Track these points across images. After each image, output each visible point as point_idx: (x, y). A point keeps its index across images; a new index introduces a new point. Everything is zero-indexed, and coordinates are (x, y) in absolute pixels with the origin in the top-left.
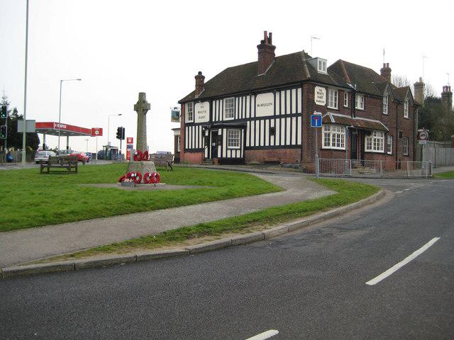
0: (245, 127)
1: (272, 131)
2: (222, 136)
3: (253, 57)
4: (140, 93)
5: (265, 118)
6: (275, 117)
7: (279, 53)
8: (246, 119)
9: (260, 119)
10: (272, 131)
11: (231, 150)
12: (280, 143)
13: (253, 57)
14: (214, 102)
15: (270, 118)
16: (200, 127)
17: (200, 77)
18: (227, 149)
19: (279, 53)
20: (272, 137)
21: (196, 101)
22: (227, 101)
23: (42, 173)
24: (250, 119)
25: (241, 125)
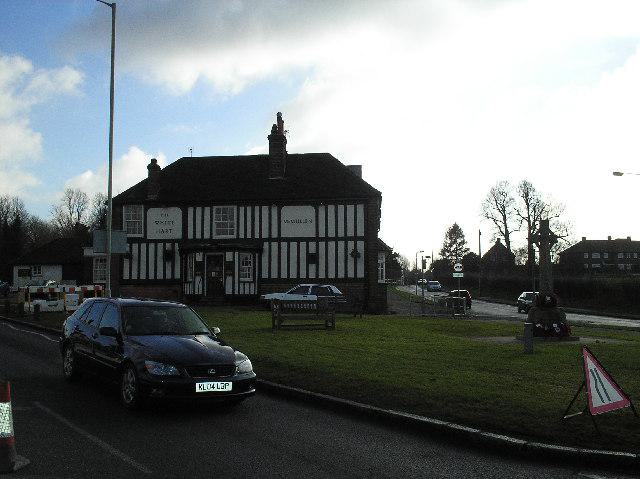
0: (260, 251)
1: (313, 259)
2: (233, 262)
3: (262, 148)
4: (360, 167)
5: (298, 240)
6: (317, 239)
7: (291, 148)
8: (261, 240)
9: (289, 240)
10: (313, 259)
11: (244, 283)
12: (279, 273)
13: (262, 148)
14: (191, 210)
15: (308, 240)
16: (160, 245)
17: (153, 166)
18: (239, 282)
19: (291, 148)
20: (169, 266)
21: (149, 205)
22: (218, 211)
23: (537, 332)
24: (270, 240)
25: (255, 247)
